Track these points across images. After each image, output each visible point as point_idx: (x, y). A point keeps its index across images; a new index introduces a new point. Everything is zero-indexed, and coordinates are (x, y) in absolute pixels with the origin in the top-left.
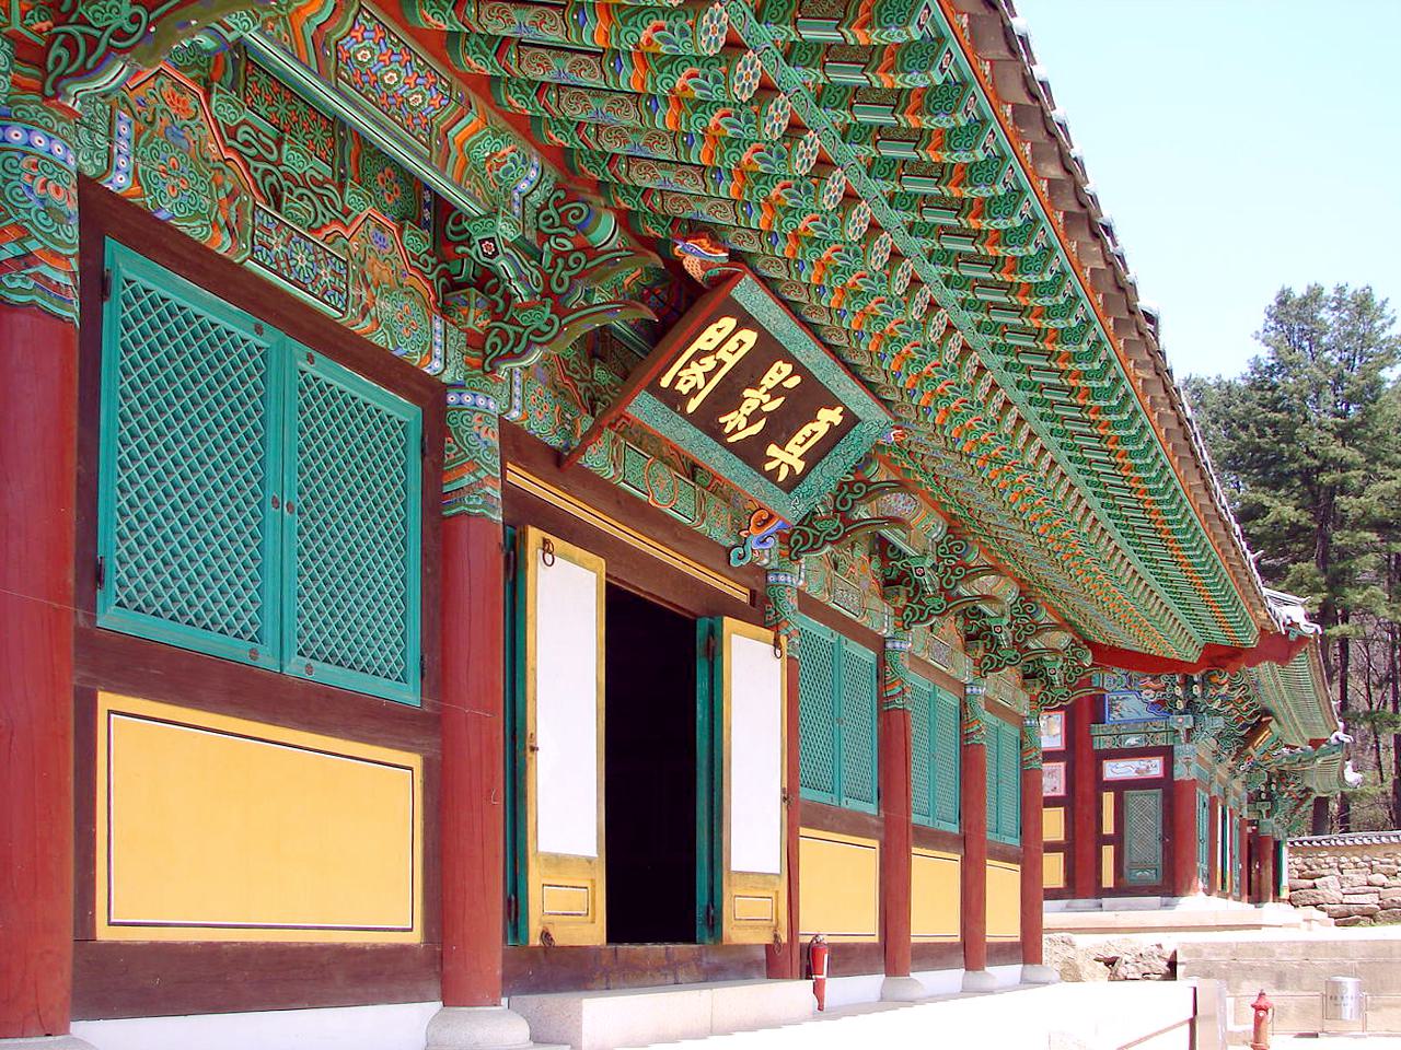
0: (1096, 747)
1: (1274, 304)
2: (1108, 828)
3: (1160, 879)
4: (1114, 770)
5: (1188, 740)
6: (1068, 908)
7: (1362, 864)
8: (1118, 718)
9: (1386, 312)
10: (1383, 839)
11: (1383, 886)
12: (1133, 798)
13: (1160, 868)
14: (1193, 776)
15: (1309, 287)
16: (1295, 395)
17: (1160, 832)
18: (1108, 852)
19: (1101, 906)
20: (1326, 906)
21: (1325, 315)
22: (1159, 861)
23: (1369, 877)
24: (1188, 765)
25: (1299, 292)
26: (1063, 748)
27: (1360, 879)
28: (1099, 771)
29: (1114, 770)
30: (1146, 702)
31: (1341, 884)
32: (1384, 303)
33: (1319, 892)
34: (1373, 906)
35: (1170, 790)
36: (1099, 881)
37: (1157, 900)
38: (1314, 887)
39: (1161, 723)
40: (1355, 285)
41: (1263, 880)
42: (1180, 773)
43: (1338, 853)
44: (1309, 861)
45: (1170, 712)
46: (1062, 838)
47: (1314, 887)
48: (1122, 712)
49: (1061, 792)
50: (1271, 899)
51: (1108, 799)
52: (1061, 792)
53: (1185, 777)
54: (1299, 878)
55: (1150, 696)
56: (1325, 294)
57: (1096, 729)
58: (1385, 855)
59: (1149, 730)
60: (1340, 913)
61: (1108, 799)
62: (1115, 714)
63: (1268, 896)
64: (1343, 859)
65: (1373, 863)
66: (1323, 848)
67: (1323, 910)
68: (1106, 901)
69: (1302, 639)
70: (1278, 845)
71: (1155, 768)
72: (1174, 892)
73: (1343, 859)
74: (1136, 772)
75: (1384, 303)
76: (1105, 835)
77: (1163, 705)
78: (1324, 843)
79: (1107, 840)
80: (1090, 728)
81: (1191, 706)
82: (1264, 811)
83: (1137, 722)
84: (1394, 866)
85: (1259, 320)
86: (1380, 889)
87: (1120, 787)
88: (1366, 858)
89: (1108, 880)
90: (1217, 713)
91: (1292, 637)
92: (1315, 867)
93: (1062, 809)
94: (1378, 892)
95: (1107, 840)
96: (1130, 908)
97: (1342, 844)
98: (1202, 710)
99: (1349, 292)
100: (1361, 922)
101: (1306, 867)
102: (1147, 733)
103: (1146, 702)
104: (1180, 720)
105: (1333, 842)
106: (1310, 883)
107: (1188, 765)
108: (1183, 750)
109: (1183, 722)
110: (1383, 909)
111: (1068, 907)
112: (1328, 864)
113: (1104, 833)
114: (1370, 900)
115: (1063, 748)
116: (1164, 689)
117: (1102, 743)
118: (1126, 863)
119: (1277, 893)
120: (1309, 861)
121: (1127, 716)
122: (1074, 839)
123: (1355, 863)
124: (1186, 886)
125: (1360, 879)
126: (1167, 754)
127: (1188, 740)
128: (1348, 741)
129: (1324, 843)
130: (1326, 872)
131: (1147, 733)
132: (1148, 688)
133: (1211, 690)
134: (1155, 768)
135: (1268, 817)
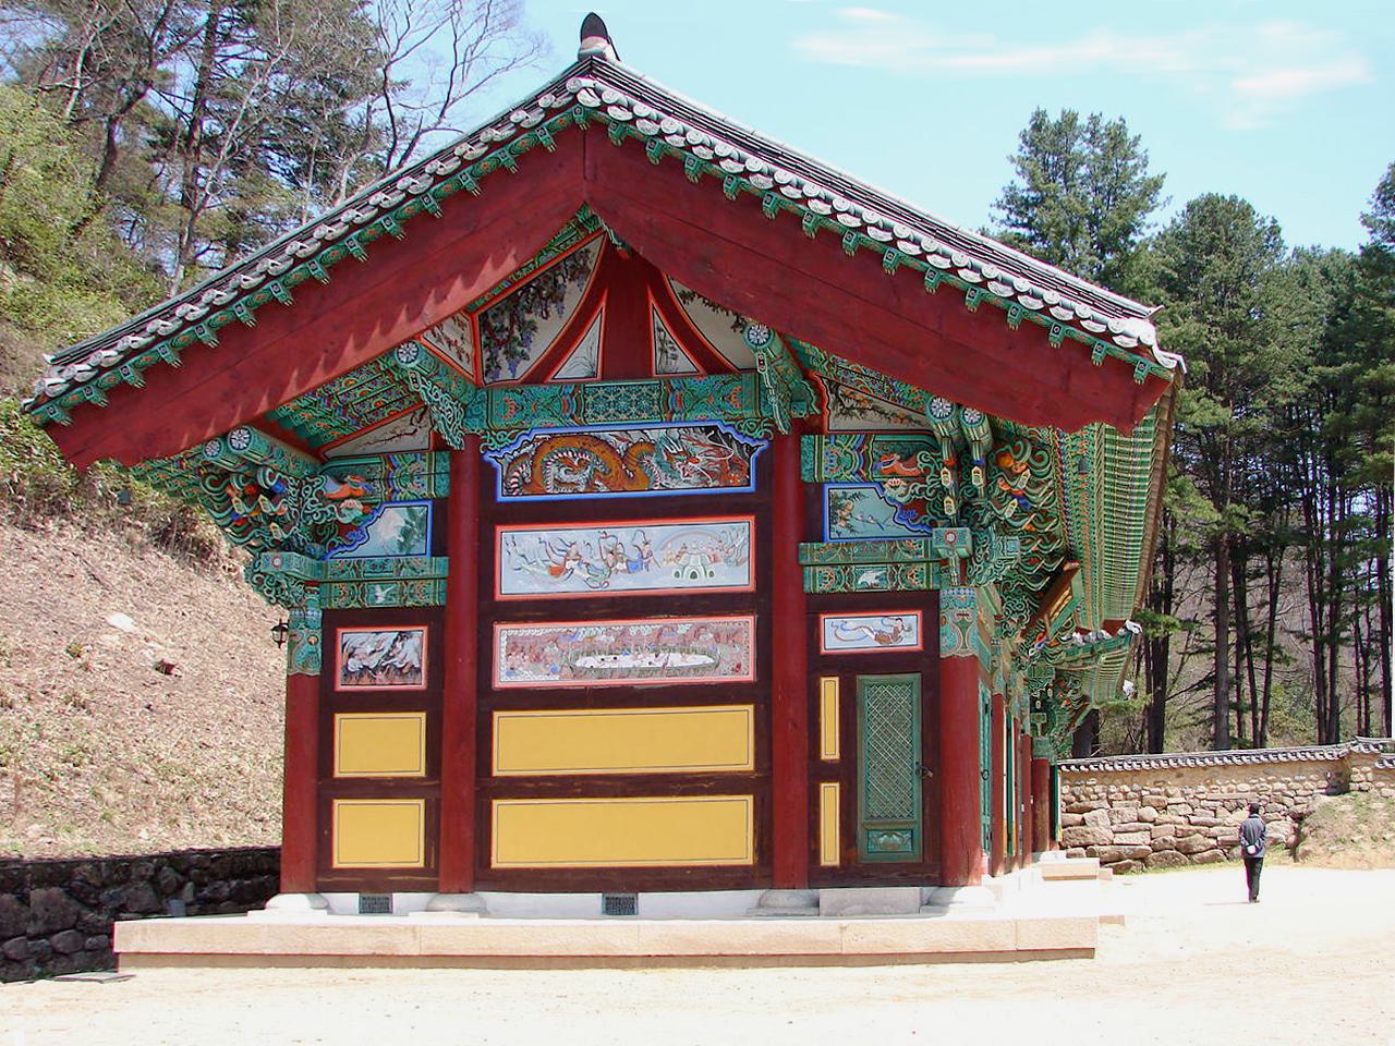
0: (808, 587)
1: (1028, 128)
2: (830, 749)
3: (918, 850)
4: (844, 634)
5: (964, 579)
6: (762, 910)
7: (1131, 794)
8: (846, 533)
9: (1139, 150)
10: (1153, 764)
11: (1153, 822)
12: (872, 686)
13: (918, 828)
14: (972, 651)
15: (1063, 112)
16: (1052, 229)
17: (917, 757)
18: (830, 794)
19: (817, 904)
20: (1096, 847)
21: (1080, 147)
22: (917, 816)
23: (1140, 811)
24: (963, 626)
25: (1054, 117)
26: (751, 588)
27: (1131, 813)
28: (813, 635)
29: (844, 634)
30: (891, 502)
31: (1111, 819)
32: (1137, 139)
33: (1088, 829)
34: (1144, 847)
35: (932, 672)
36: (815, 854)
37: (910, 894)
38: (1083, 823)
39: (917, 545)
40: (1109, 118)
41: (1039, 822)
42: (952, 643)
43: (1106, 780)
44: (1077, 790)
45: (933, 524)
46: (750, 767)
47: (1083, 823)
48: (852, 522)
49: (748, 675)
50: (1048, 848)
51: (830, 688)
52: (748, 675)
53: (958, 652)
54: (1067, 812)
55: (899, 491)
56: (1078, 123)
57: (810, 552)
58: (1155, 782)
59: (897, 558)
60: (1111, 856)
61: (830, 688)
62: (840, 526)
63: (1044, 840)
64: (1113, 789)
65: (1144, 793)
66: (1090, 774)
67: (1091, 854)
68: (828, 895)
69: (1154, 381)
70: (1053, 769)
71: (906, 631)
72: (942, 876)
73: (1113, 789)
74: (877, 638)
75: (1137, 139)
76: (825, 762)
77: (920, 511)
78: (1092, 767)
79: (828, 772)
80: (797, 550)
81: (968, 514)
82: (1039, 725)
83: (879, 540)
84: (1164, 798)
85: (1014, 146)
86: (1151, 826)
87: (851, 667)
88: (1136, 787)
89: (830, 854)
90: (1005, 528)
91: (1140, 376)
92: (1083, 798)
93: (750, 708)
94: (1150, 830)
95: (828, 772)
96: (869, 911)
97: (1285, 760)
98: (985, 521)
99: (1103, 123)
100: (1133, 868)
101: (1074, 798)
102: (896, 564)
103: (891, 502)
104: (951, 538)
105: (1101, 766)
106: (1078, 817)
107: (963, 626)
108: (956, 599)
109: (954, 542)
110: (1154, 851)
111: (760, 906)
112: (1097, 794)
113: (823, 757)
114: (1141, 840)
115: (751, 588)
116: (921, 478)
117: (819, 581)
118: (861, 817)
119: (1053, 837)
120: (1077, 790)
121: (863, 529)
122: (771, 768)
123: (1125, 793)
124: (963, 867)
125: (1131, 813)
126: (927, 604)
127: (964, 579)
128: (1137, 631)
129: (1092, 767)
130: (1094, 804)
131: (896, 564)
132: (894, 474)
133: (1000, 482)
134: (906, 631)
135: (1043, 734)
